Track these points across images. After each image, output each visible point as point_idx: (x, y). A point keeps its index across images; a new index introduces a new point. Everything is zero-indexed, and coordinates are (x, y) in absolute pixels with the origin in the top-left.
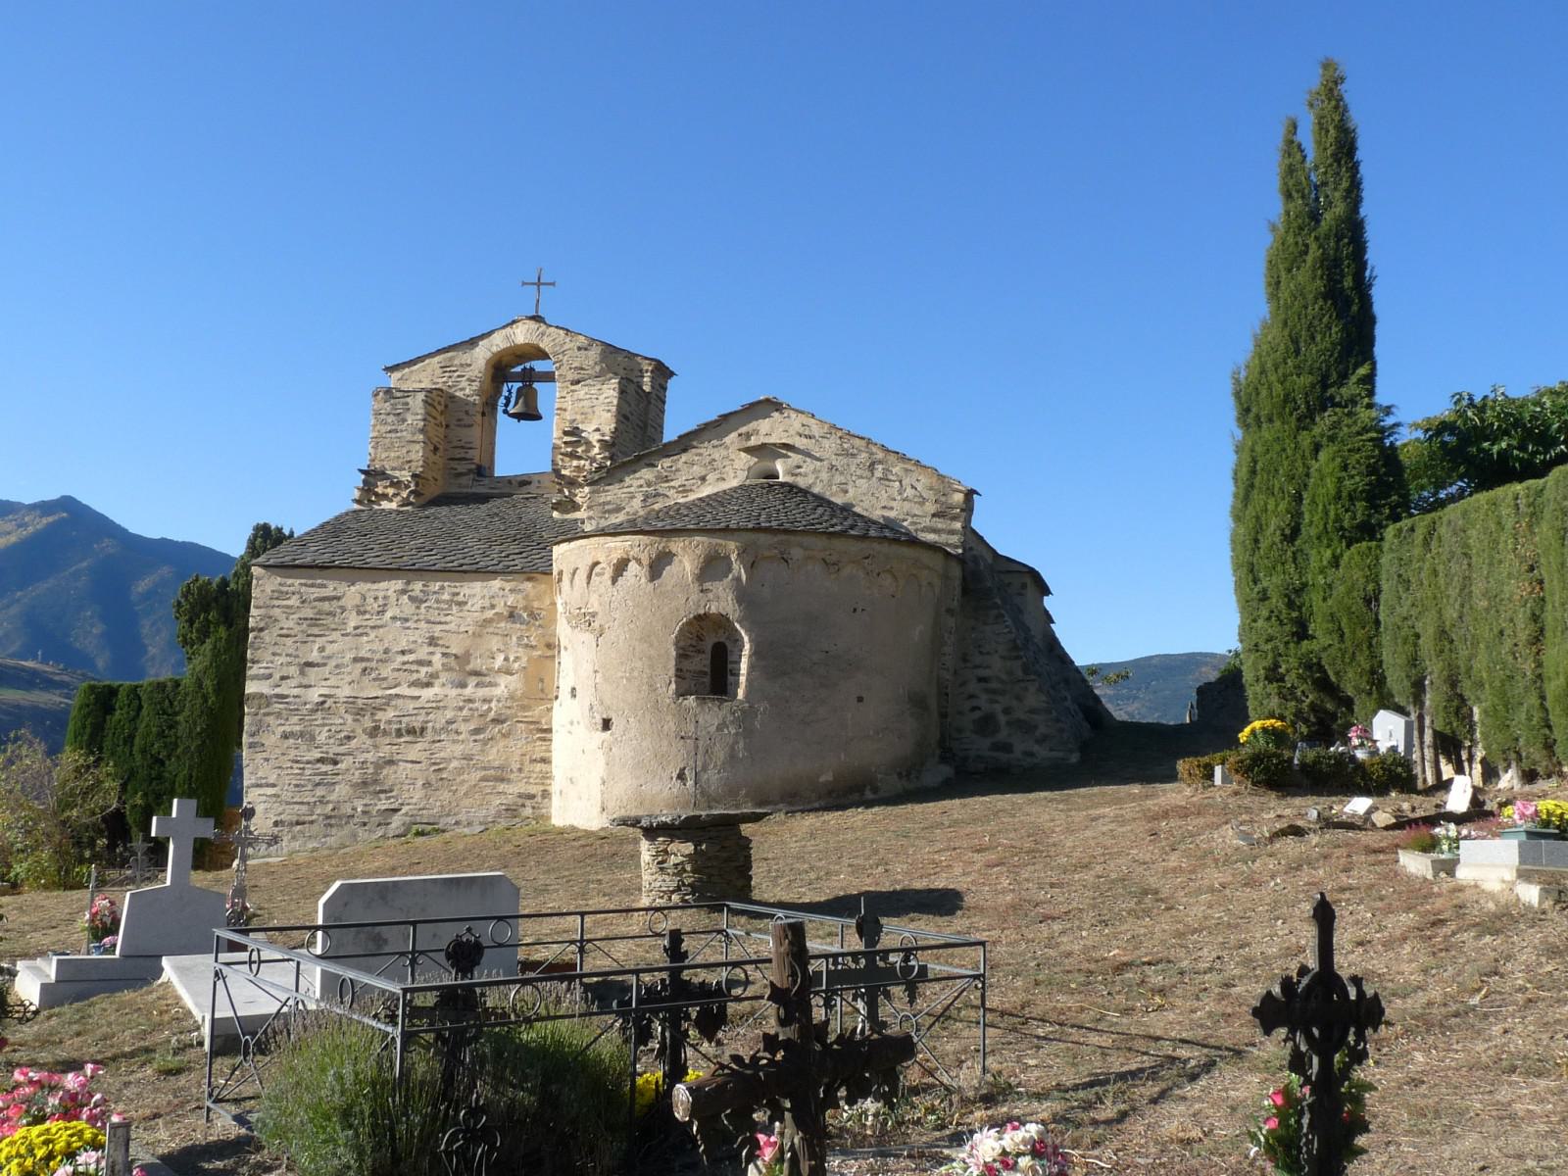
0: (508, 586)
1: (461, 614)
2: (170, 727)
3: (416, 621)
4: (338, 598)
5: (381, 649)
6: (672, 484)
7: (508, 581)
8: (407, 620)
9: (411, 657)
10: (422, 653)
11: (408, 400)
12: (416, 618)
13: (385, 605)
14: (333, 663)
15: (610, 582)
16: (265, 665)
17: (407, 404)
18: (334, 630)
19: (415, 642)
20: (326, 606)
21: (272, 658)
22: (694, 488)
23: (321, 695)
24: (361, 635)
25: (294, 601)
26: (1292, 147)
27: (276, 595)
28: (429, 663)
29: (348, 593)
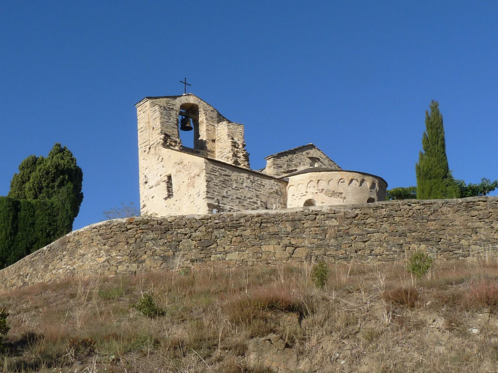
0: (276, 183)
1: (264, 189)
2: (54, 222)
3: (252, 189)
4: (230, 176)
5: (244, 196)
6: (293, 163)
7: (275, 181)
8: (250, 188)
9: (252, 200)
10: (255, 199)
11: (171, 112)
12: (252, 188)
13: (243, 181)
14: (230, 198)
15: (347, 185)
16: (211, 194)
17: (170, 113)
18: (229, 187)
19: (252, 195)
20: (226, 178)
21: (213, 192)
22: (298, 165)
23: (229, 208)
24: (237, 190)
25: (217, 174)
26: (427, 113)
27: (212, 170)
28: (257, 203)
29: (232, 175)
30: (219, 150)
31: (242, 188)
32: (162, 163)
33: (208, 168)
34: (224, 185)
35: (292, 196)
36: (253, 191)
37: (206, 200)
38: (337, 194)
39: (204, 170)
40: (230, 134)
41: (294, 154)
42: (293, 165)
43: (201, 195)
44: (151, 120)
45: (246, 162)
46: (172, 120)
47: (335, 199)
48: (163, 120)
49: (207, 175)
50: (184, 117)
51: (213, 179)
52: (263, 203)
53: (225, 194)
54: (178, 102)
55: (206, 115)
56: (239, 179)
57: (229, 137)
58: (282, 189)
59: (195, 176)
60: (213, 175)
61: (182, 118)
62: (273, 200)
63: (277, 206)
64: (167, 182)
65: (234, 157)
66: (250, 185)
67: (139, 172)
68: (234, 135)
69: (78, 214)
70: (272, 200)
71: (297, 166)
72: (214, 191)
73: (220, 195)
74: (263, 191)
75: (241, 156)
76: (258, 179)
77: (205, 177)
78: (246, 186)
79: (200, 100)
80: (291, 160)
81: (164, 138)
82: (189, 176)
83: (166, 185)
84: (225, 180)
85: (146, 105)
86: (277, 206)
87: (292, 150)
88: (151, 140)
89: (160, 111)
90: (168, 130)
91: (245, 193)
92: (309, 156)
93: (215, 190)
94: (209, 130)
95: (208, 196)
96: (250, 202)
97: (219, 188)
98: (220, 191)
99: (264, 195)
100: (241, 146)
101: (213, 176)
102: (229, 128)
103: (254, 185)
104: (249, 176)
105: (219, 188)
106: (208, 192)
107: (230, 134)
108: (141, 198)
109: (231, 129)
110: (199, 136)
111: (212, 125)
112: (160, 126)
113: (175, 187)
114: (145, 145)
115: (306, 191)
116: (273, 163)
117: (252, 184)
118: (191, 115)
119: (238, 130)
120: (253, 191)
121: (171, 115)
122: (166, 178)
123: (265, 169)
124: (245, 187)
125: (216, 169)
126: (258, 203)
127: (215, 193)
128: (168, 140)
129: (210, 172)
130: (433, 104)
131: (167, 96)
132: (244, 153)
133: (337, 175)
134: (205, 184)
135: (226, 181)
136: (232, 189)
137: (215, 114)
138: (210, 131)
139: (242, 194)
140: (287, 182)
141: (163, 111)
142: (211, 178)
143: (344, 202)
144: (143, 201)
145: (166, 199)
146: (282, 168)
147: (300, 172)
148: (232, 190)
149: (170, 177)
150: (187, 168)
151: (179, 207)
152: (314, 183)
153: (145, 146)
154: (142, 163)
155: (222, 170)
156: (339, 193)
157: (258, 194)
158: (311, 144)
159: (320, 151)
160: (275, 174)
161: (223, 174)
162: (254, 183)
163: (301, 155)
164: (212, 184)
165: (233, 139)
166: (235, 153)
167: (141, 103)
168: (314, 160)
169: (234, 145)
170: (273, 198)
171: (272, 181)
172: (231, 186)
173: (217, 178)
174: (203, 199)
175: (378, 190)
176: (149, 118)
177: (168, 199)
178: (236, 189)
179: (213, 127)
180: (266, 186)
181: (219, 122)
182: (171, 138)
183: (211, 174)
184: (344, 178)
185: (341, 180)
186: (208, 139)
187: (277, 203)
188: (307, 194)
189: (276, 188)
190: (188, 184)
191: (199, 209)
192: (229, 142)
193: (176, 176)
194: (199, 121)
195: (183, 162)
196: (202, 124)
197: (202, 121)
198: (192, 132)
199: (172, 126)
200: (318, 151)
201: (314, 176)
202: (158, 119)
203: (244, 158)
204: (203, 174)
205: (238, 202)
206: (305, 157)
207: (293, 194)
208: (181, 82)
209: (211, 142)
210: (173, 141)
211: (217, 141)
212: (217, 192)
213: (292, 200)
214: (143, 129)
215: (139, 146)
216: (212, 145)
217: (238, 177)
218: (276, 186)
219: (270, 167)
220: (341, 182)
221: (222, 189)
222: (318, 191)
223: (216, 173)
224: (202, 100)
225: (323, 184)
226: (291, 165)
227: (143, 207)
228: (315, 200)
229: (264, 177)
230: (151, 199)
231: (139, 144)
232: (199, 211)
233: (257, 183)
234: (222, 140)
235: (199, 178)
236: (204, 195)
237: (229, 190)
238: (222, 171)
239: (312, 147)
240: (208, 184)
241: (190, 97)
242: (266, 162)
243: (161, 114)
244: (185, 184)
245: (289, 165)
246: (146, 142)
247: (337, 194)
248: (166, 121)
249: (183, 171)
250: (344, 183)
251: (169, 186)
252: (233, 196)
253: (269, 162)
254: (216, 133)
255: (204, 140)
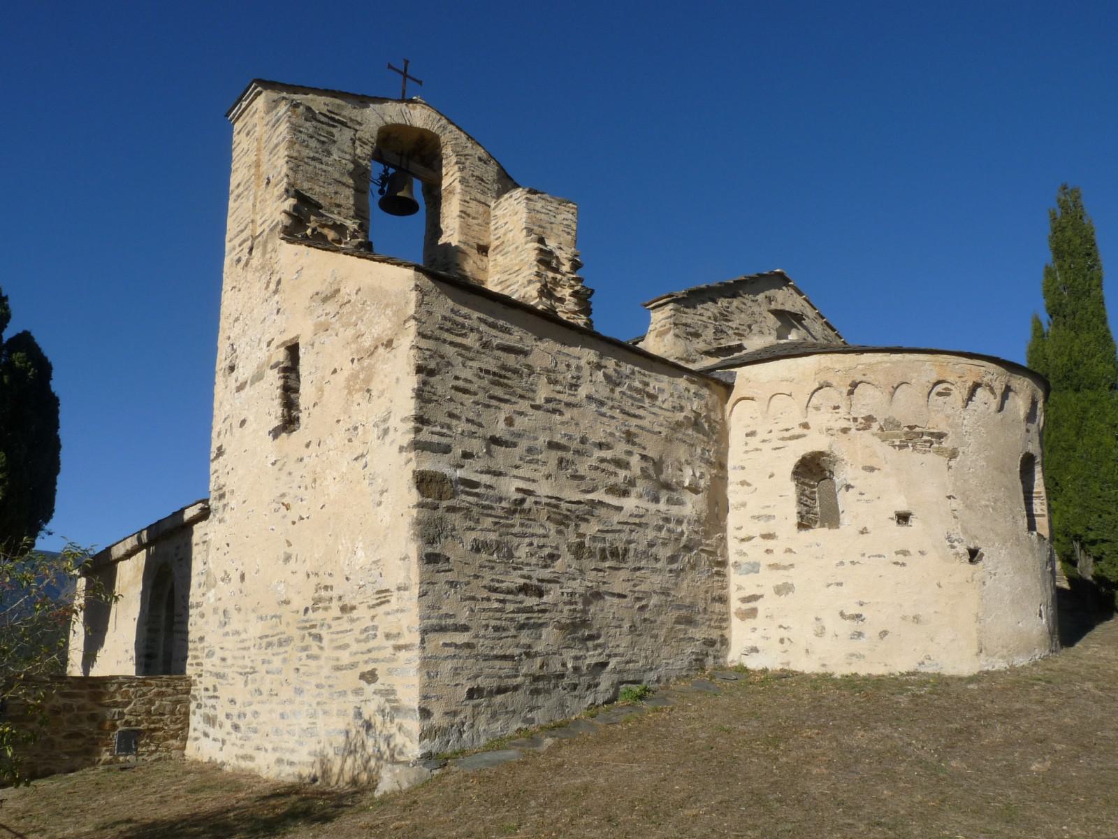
0: (693, 388)
3: (612, 408)
5: (578, 436)
6: (730, 324)
7: (692, 382)
8: (602, 404)
9: (608, 454)
10: (619, 450)
11: (334, 130)
12: (610, 403)
14: (524, 444)
15: (960, 403)
16: (438, 429)
18: (522, 397)
19: (612, 434)
20: (511, 360)
21: (448, 420)
22: (746, 333)
23: (518, 490)
24: (554, 411)
25: (471, 340)
27: (448, 325)
28: (626, 465)
29: (536, 350)
30: (498, 276)
31: (574, 406)
32: (277, 297)
33: (430, 313)
34: (499, 392)
35: (747, 435)
36: (613, 418)
37: (412, 455)
38: (925, 438)
39: (413, 323)
40: (535, 228)
41: (734, 296)
42: (730, 332)
43: (392, 430)
44: (265, 157)
45: (583, 316)
46: (335, 156)
47: (918, 457)
48: (298, 151)
49: (425, 344)
50: (391, 171)
51: (449, 364)
52: (649, 465)
53: (500, 429)
54: (375, 117)
55: (461, 170)
56: (562, 367)
57: (527, 236)
58: (714, 409)
59: (376, 347)
60: (451, 343)
61: (386, 171)
62: (682, 452)
63: (698, 474)
64: (285, 370)
65: (544, 299)
66: (603, 391)
67: (218, 332)
68: (548, 232)
69: (61, 466)
70: (681, 452)
71: (743, 336)
72: (451, 415)
73: (481, 432)
74: (650, 417)
75: (568, 298)
76: (633, 373)
77: (414, 352)
78: (589, 398)
79: (444, 121)
80: (725, 316)
81: (295, 208)
82: (354, 346)
83: (280, 383)
84: (504, 367)
85: (254, 110)
86: (698, 474)
87: (728, 285)
88: (259, 222)
89: (292, 120)
90: (317, 189)
91: (585, 423)
92: (773, 306)
93: (457, 412)
94: (469, 215)
95: (425, 436)
96: (603, 460)
97: (477, 403)
98: (479, 415)
99: (653, 433)
100: (566, 267)
101: (450, 351)
102: (532, 207)
103: (617, 395)
104: (601, 356)
105: (477, 403)
106: (421, 420)
107: (535, 228)
108: (214, 423)
109: (538, 212)
110: (439, 233)
111: (480, 202)
112: (285, 170)
113: (306, 395)
114: (239, 242)
115: (804, 421)
116: (671, 320)
117: (612, 391)
118: (415, 166)
119: (560, 217)
120: (613, 418)
121: (334, 142)
122: (281, 355)
123: (642, 339)
124: (585, 402)
125: (467, 322)
126: (632, 464)
127: (454, 422)
128: (312, 218)
129: (437, 333)
130: (1065, 194)
131: (333, 91)
132: (577, 288)
133: (925, 368)
134: (412, 381)
135: (509, 374)
136: (533, 407)
137: (490, 172)
138: (474, 218)
139: (571, 430)
140: (729, 387)
141: (301, 121)
142: (442, 357)
143: (950, 468)
144: (219, 434)
145: (276, 433)
146: (701, 339)
147: (753, 353)
148: (531, 411)
149: (293, 350)
150: (351, 313)
151: (315, 472)
152: (835, 395)
153: (240, 245)
154: (230, 302)
155: (493, 326)
156: (932, 434)
157: (633, 430)
158: (778, 270)
159: (800, 294)
160: (678, 355)
161: (495, 342)
162: (618, 385)
163: (753, 301)
164: (442, 384)
165: (541, 240)
166: (549, 285)
167: (244, 104)
168: (788, 319)
169: (546, 259)
170: (684, 442)
171: (682, 382)
172: (531, 395)
173: (472, 360)
174: (401, 449)
175: (1041, 424)
176: (259, 150)
177: (284, 435)
178: (551, 406)
179: (481, 209)
180: (660, 399)
181: (499, 194)
182: (323, 215)
183: (445, 341)
184: (951, 379)
185: (939, 387)
186: (465, 243)
187: (698, 463)
188: (805, 431)
189: (694, 408)
190: (348, 380)
191: (382, 493)
192: (530, 252)
193: (313, 345)
194: (443, 188)
195: (338, 291)
196: (450, 196)
197: (450, 189)
198: (418, 220)
199: (337, 175)
200: (795, 295)
201: (838, 367)
202: (284, 145)
203: (576, 304)
204: (408, 339)
205: (553, 463)
206: (764, 308)
207: (749, 430)
208: (390, 67)
209: (476, 251)
210: (330, 223)
211: (493, 251)
212: (468, 420)
213: (746, 452)
214: (241, 188)
215: (228, 246)
216: (479, 263)
217: (562, 358)
218: (695, 401)
219: (661, 334)
220: (939, 394)
221: (488, 406)
222: (851, 424)
223: (464, 335)
224: (453, 124)
225: (870, 400)
226: (726, 330)
227: (218, 456)
228: (840, 456)
229: (655, 365)
230: (237, 430)
231: (227, 238)
232: (380, 504)
233: (630, 388)
234: (511, 241)
235: (391, 356)
236: (403, 433)
237: (521, 414)
238: (494, 332)
239: (781, 280)
240: (425, 383)
241: (414, 108)
242: (650, 318)
243: (295, 129)
244: (341, 378)
245: (719, 332)
246: (245, 228)
247: (925, 438)
248: (312, 155)
249: (338, 325)
250: (948, 398)
251: (292, 383)
252: (536, 439)
253: (659, 318)
254: (493, 228)
255: (453, 245)
